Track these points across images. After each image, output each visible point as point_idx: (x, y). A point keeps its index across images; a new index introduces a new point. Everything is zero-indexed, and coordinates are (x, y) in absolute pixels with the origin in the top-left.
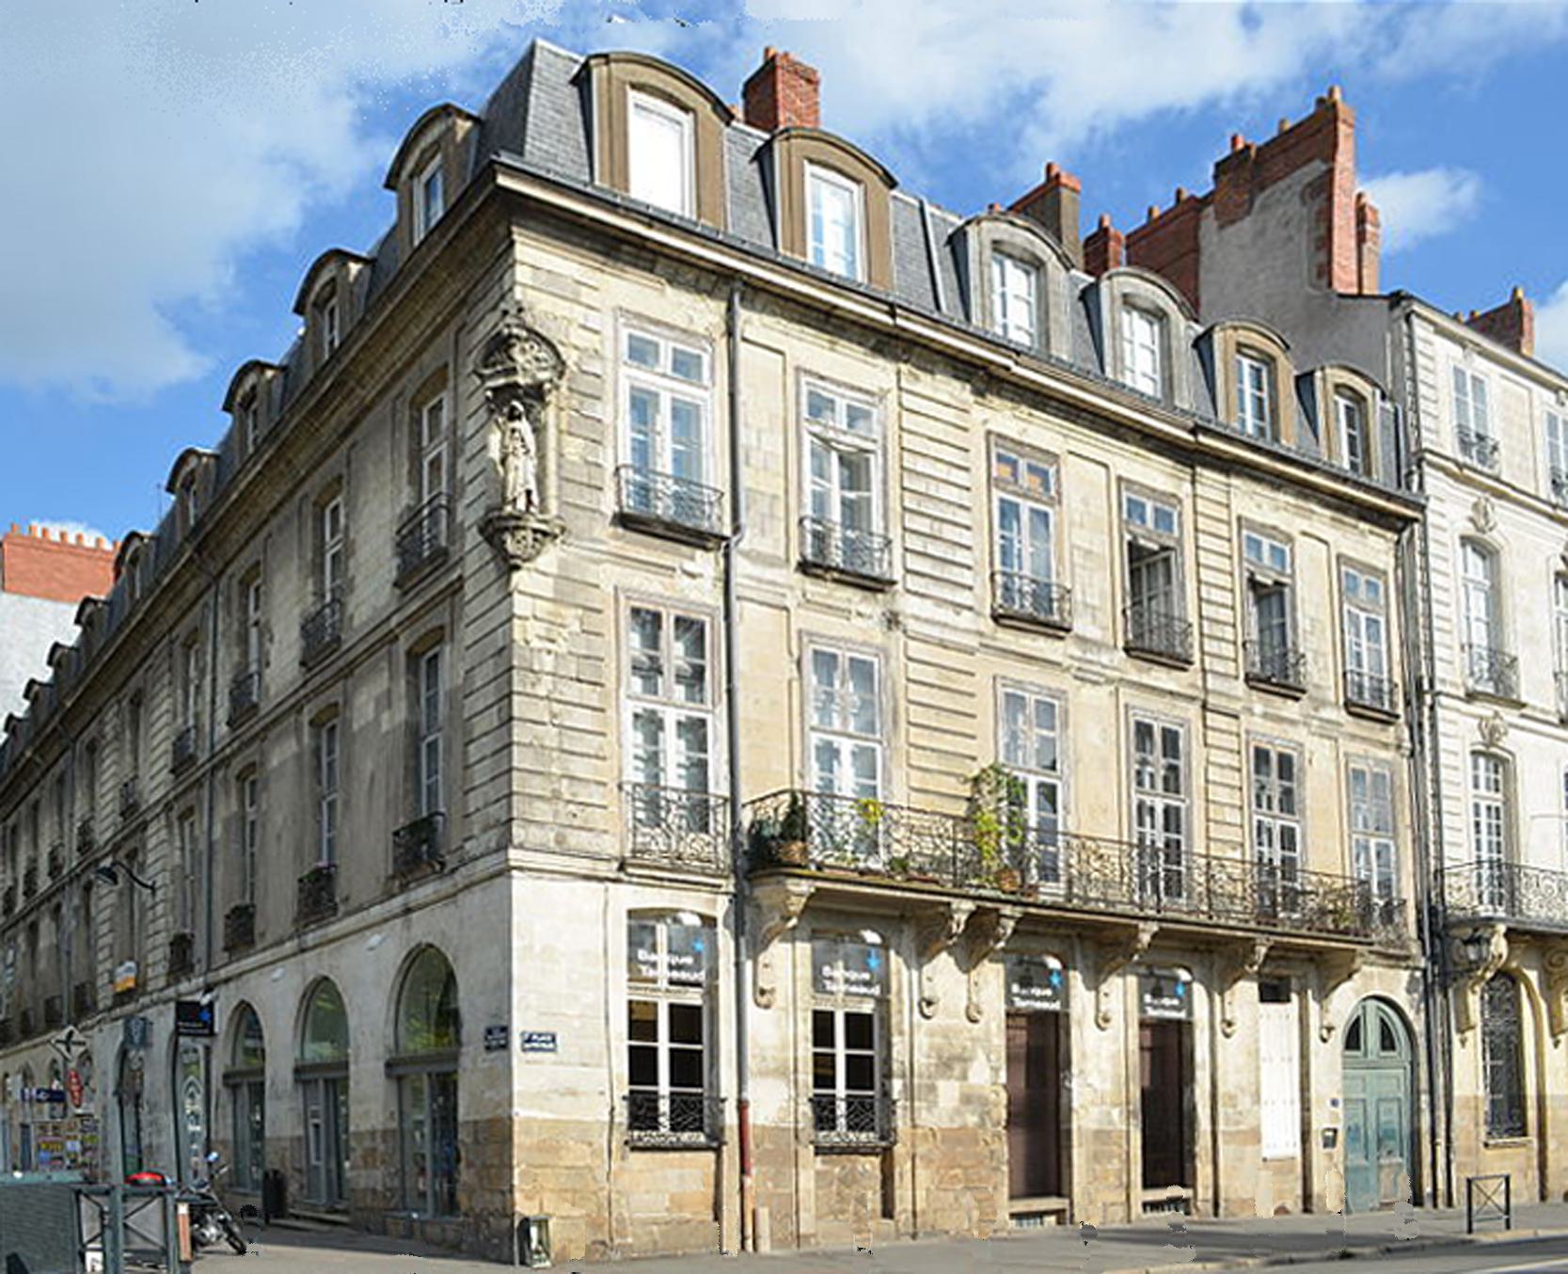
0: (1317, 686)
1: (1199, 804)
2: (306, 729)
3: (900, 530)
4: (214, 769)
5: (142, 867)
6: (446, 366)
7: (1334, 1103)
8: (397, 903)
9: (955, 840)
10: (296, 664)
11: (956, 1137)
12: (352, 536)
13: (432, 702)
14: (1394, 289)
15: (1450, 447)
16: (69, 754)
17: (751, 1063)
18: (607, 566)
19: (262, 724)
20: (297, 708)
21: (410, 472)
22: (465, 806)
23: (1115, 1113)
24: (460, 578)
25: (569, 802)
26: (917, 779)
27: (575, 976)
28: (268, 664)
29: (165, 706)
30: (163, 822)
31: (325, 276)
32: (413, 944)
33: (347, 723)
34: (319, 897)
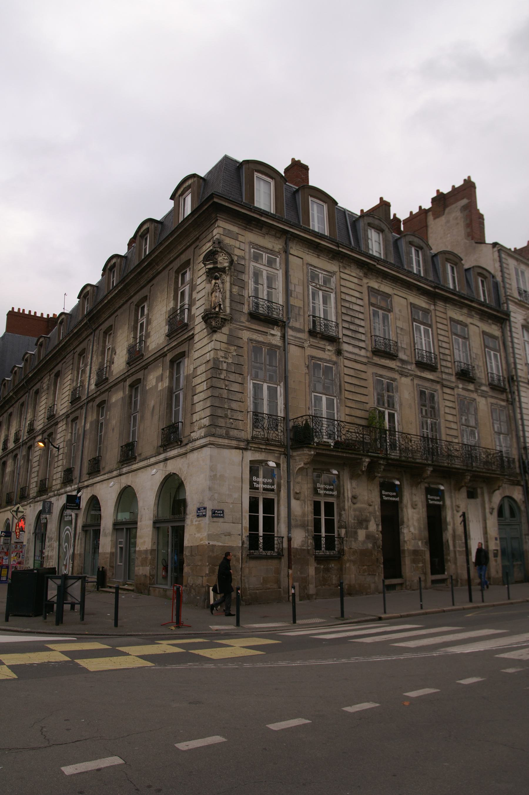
0: (479, 378)
1: (442, 421)
2: (127, 388)
3: (341, 321)
4: (88, 402)
5: (54, 440)
6: (190, 259)
7: (496, 539)
8: (162, 457)
9: (363, 434)
10: (125, 363)
11: (364, 553)
12: (150, 317)
13: (178, 379)
14: (494, 241)
15: (516, 295)
16: (27, 394)
17: (293, 523)
18: (245, 331)
19: (110, 385)
20: (124, 380)
21: (174, 295)
22: (192, 419)
23: (420, 543)
24: (193, 334)
25: (230, 419)
26: (348, 411)
27: (231, 487)
28: (113, 363)
29: (69, 377)
30: (64, 423)
31: (145, 227)
32: (167, 473)
33: (144, 386)
34: (129, 455)
